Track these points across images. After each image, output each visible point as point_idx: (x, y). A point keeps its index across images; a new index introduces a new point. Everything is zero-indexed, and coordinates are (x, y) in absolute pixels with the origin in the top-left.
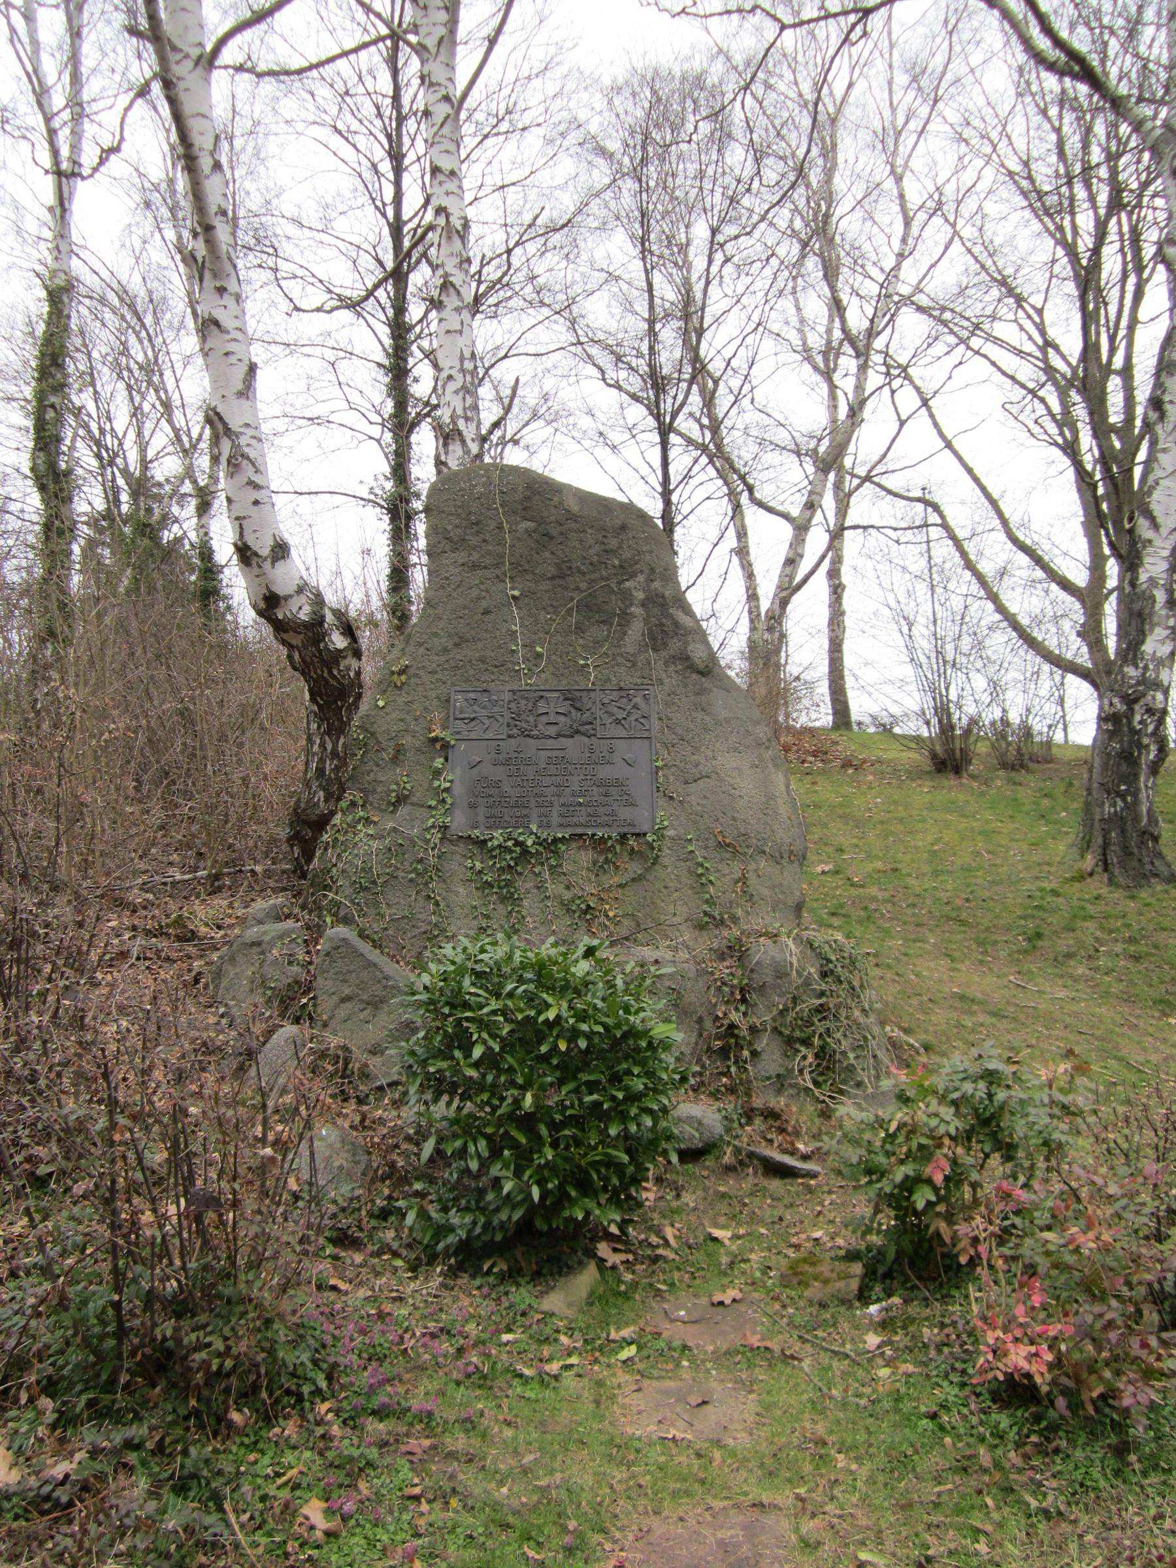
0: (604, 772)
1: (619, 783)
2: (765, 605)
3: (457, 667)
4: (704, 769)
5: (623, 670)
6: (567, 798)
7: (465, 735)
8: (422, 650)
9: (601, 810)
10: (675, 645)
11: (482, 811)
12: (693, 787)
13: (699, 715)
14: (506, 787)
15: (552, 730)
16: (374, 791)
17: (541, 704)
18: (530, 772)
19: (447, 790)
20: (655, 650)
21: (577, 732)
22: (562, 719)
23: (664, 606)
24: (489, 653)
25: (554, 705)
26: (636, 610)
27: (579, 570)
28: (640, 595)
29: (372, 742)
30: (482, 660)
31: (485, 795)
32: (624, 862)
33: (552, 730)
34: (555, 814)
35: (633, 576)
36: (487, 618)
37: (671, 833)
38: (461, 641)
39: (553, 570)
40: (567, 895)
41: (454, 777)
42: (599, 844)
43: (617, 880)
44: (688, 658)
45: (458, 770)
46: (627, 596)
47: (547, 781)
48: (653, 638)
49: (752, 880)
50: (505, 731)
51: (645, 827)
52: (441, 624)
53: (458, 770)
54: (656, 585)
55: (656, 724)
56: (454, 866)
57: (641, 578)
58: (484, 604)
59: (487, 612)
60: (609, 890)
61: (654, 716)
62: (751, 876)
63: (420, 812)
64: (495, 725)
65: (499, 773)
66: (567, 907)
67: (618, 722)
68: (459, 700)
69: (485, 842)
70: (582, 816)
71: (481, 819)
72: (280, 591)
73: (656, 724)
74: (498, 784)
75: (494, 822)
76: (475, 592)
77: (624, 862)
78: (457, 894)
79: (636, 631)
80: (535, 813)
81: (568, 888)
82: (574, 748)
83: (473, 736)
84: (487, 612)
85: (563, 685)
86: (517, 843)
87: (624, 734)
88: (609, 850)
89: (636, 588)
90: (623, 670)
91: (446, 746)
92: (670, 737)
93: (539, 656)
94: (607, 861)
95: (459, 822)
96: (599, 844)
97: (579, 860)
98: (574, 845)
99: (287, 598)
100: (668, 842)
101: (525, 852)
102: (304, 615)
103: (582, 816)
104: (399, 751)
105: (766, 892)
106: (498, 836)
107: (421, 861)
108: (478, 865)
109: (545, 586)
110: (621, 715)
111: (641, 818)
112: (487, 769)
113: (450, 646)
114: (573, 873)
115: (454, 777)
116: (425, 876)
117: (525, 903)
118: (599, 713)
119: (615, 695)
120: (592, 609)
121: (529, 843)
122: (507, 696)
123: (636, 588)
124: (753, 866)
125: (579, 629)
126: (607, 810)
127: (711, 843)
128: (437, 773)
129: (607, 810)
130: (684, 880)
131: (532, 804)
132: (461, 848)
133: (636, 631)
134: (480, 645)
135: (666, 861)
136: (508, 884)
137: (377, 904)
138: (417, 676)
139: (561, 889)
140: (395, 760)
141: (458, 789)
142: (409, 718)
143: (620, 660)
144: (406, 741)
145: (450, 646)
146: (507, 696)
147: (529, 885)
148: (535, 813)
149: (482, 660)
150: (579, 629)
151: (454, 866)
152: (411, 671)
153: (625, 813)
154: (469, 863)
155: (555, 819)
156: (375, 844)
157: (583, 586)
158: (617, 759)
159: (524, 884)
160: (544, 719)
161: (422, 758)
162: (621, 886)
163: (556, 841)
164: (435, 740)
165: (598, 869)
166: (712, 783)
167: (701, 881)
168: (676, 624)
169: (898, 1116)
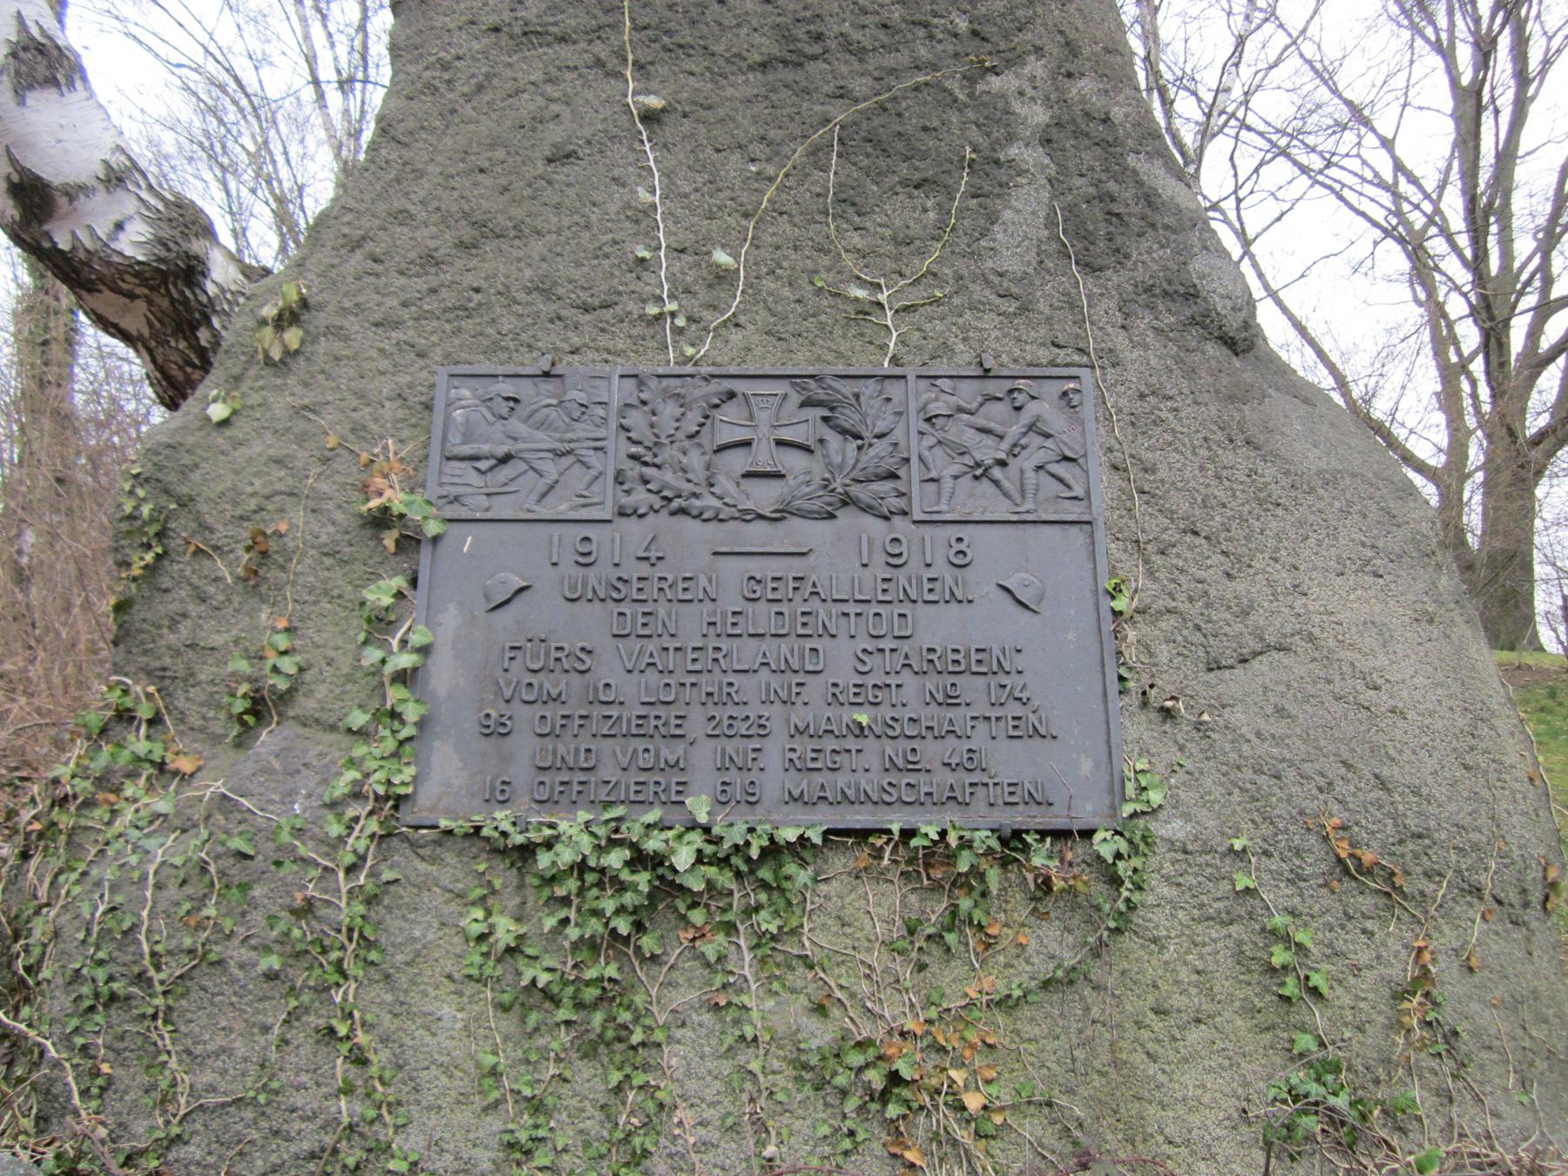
0: (938, 628)
1: (988, 663)
2: (1466, 80)
3: (466, 311)
4: (1275, 621)
5: (989, 321)
6: (814, 709)
7: (476, 505)
8: (357, 261)
9: (931, 751)
10: (1148, 257)
11: (525, 747)
12: (1236, 681)
13: (1238, 459)
14: (609, 669)
15: (764, 496)
16: (190, 679)
17: (731, 411)
18: (690, 625)
19: (402, 677)
20: (1090, 268)
21: (847, 501)
22: (793, 461)
23: (1109, 146)
24: (563, 269)
25: (772, 415)
26: (1029, 156)
27: (847, 44)
28: (1039, 115)
29: (182, 527)
30: (544, 289)
31: (534, 689)
32: (1009, 913)
33: (764, 496)
34: (774, 753)
35: (1013, 60)
36: (561, 174)
37: (1171, 828)
38: (481, 233)
39: (767, 46)
40: (819, 1035)
41: (446, 634)
42: (929, 862)
43: (994, 982)
44: (1191, 295)
45: (450, 618)
46: (997, 117)
47: (747, 652)
48: (1081, 233)
49: (1449, 980)
50: (607, 497)
51: (1086, 812)
52: (421, 190)
53: (450, 618)
54: (1085, 88)
55: (1104, 486)
56: (424, 929)
57: (1035, 67)
58: (554, 134)
59: (562, 156)
60: (962, 1017)
61: (1097, 465)
62: (1444, 969)
63: (321, 745)
64: (577, 479)
65: (590, 625)
66: (814, 1074)
67: (980, 473)
68: (463, 405)
69: (527, 851)
70: (867, 767)
71: (521, 774)
72: (53, 169)
73: (1104, 486)
74: (580, 661)
75: (565, 783)
76: (529, 104)
77: (1009, 913)
78: (432, 1023)
79: (1026, 213)
80: (704, 757)
81: (820, 1010)
82: (839, 551)
83: (502, 508)
84: (562, 156)
85: (801, 363)
86: (640, 859)
87: (1002, 510)
88: (959, 883)
89: (1024, 94)
90: (989, 321)
91: (410, 542)
92: (1152, 524)
93: (723, 277)
94: (954, 919)
95: (446, 784)
96: (929, 862)
97: (856, 912)
98: (838, 862)
99: (74, 192)
100: (1161, 861)
101: (668, 887)
102: (134, 243)
103: (867, 767)
104: (262, 551)
105: (1496, 1023)
106: (574, 833)
107: (306, 910)
108: (505, 930)
109: (747, 85)
110: (988, 451)
111: (1072, 782)
112: (546, 614)
113: (444, 245)
114: (840, 959)
115: (446, 634)
116: (324, 958)
117: (672, 1058)
118: (915, 447)
119: (969, 392)
120: (879, 144)
121: (683, 858)
122: (618, 392)
123: (1024, 94)
124: (1447, 937)
125: (849, 202)
126: (953, 749)
127: (1315, 865)
128: (381, 624)
129: (953, 749)
130: (1222, 986)
131: (697, 724)
132: (451, 869)
133: (1026, 213)
134: (538, 247)
135: (1157, 920)
136: (609, 993)
137: (153, 1059)
138: (334, 331)
139: (794, 1013)
140: (252, 579)
141: (444, 676)
142: (302, 457)
143: (978, 291)
144: (294, 523)
145: (444, 249)
146: (618, 392)
147: (685, 996)
148: (704, 757)
149: (544, 289)
150: (849, 202)
151: (424, 929)
152: (321, 319)
153: (1011, 762)
154: (474, 921)
155: (774, 780)
156: (162, 848)
157: (860, 86)
158: (980, 583)
159: (670, 994)
160: (738, 461)
161: (338, 579)
162: (1004, 1003)
163: (773, 851)
164: (381, 520)
165: (922, 944)
166: (1297, 666)
167: (1285, 988)
168: (1150, 198)
169: (474, 262)
